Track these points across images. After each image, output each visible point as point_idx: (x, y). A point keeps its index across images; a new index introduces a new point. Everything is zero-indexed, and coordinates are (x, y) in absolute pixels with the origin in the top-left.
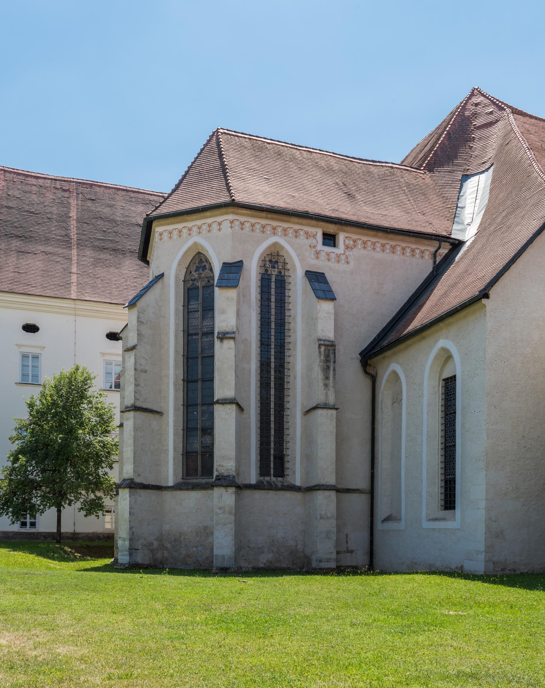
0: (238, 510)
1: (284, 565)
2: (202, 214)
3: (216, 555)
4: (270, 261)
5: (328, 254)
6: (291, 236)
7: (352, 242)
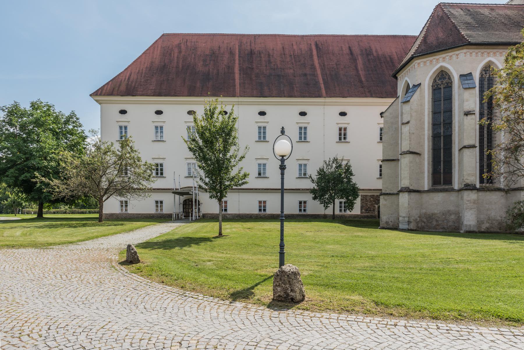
1: (495, 230)
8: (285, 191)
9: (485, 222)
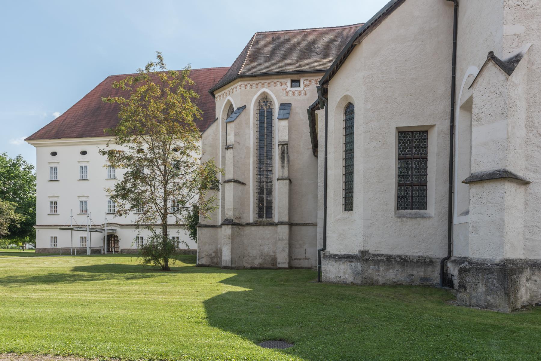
0: (233, 237)
1: (268, 266)
4: (264, 102)
5: (293, 92)
7: (308, 82)
8: (168, 227)
9: (258, 258)
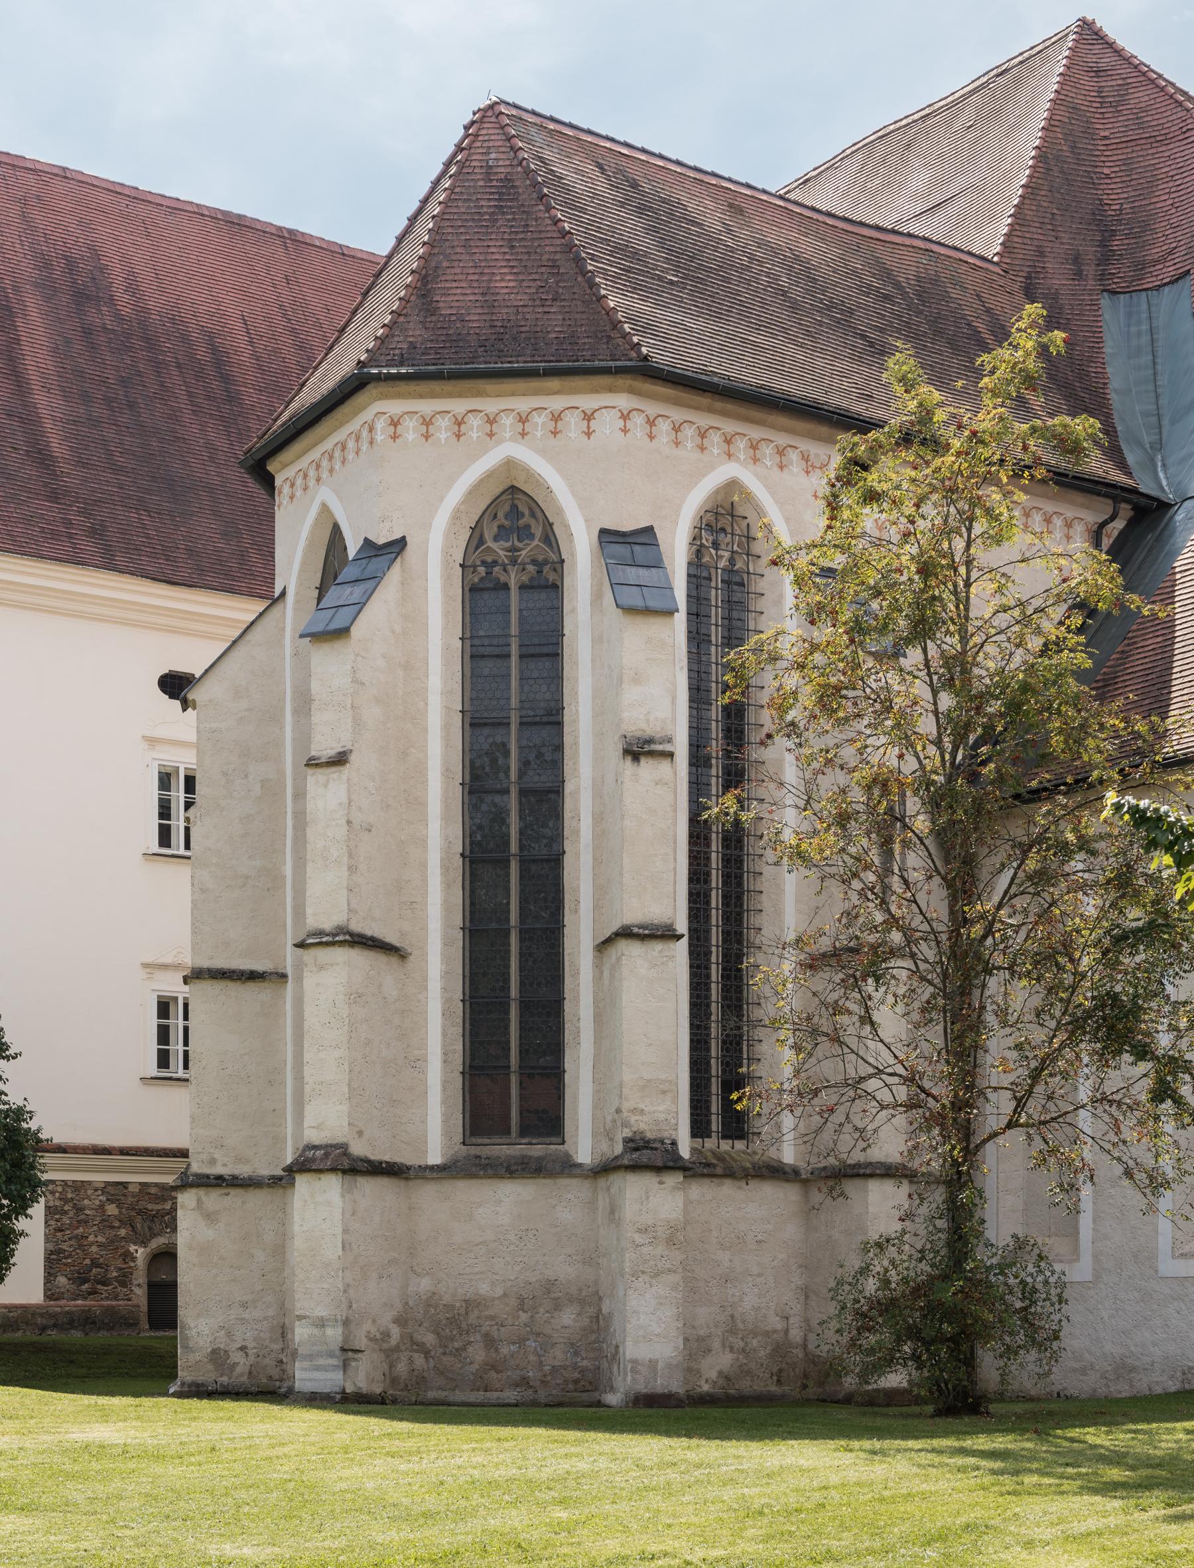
2: (535, 383)
3: (635, 1362)
6: (769, 464)
9: (716, 1344)
